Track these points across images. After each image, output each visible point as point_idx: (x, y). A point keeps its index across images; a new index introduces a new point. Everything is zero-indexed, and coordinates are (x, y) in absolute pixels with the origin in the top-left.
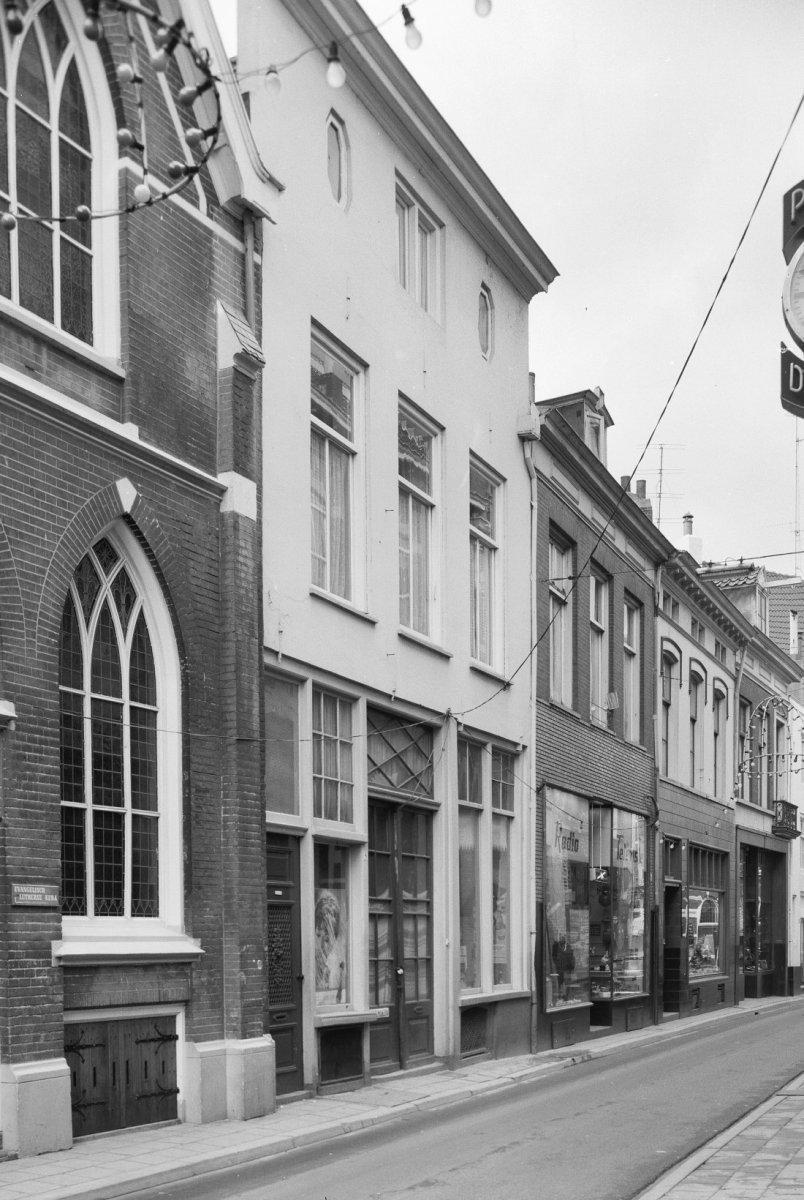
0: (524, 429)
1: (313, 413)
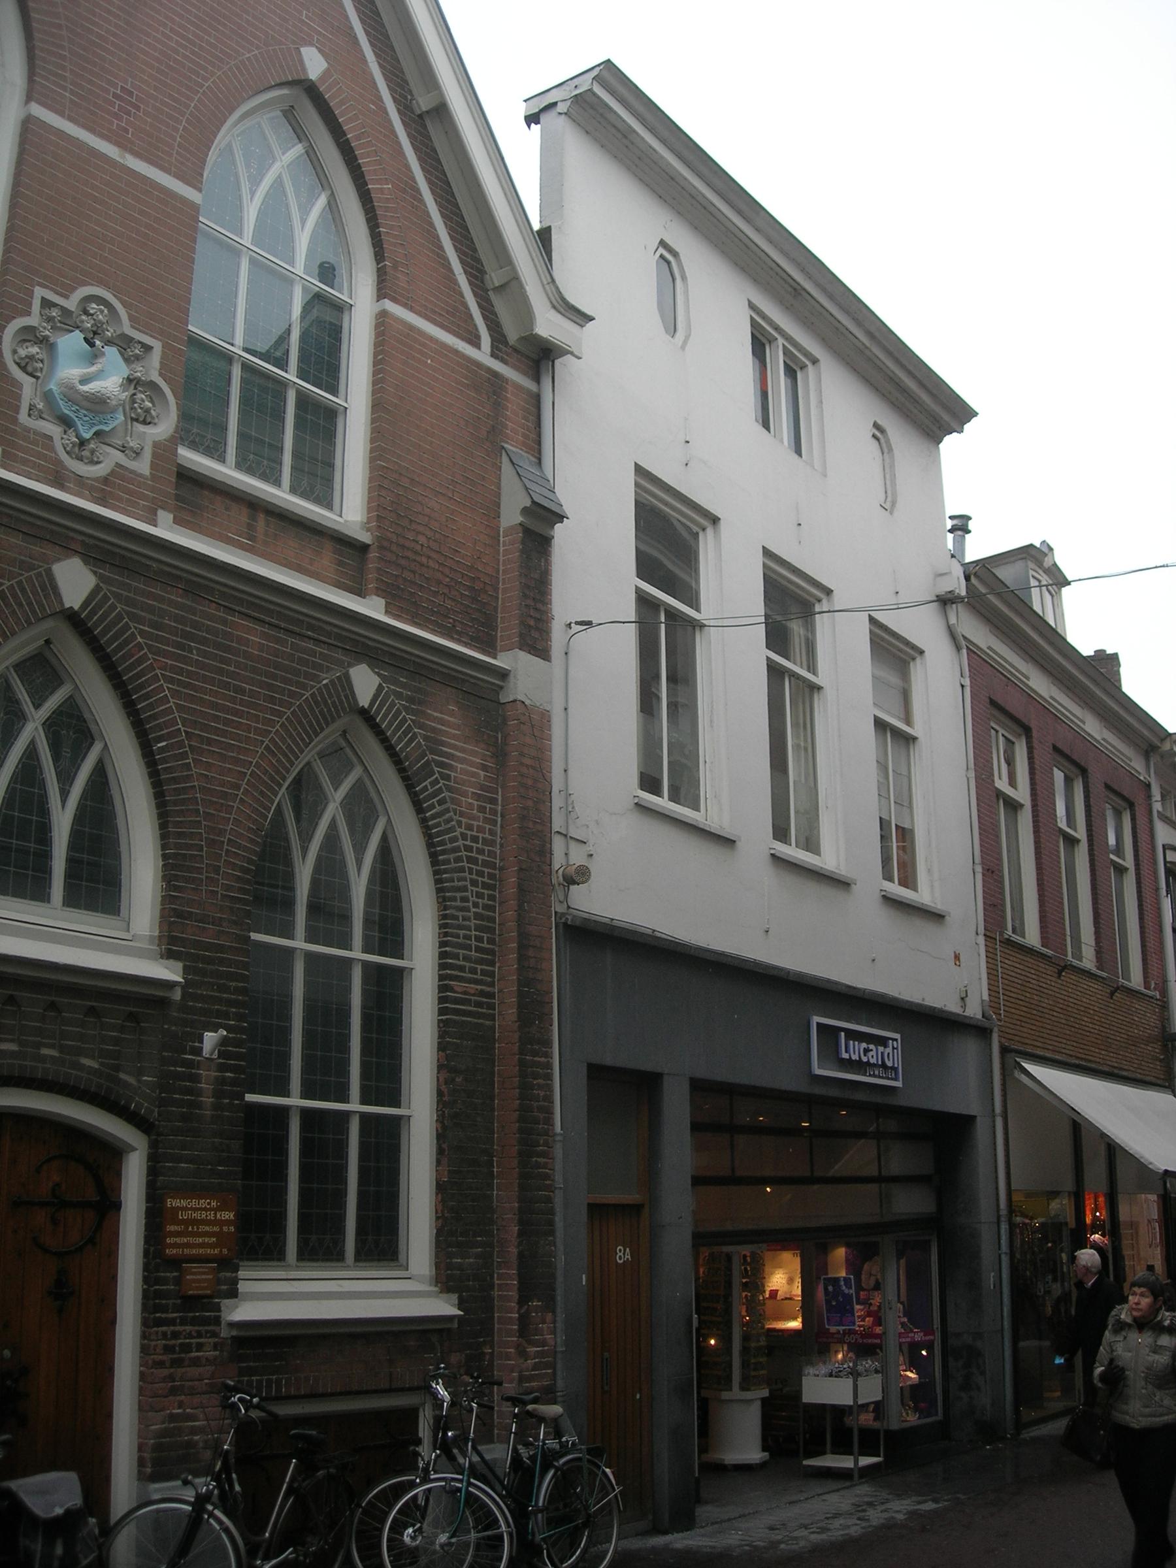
0: (944, 587)
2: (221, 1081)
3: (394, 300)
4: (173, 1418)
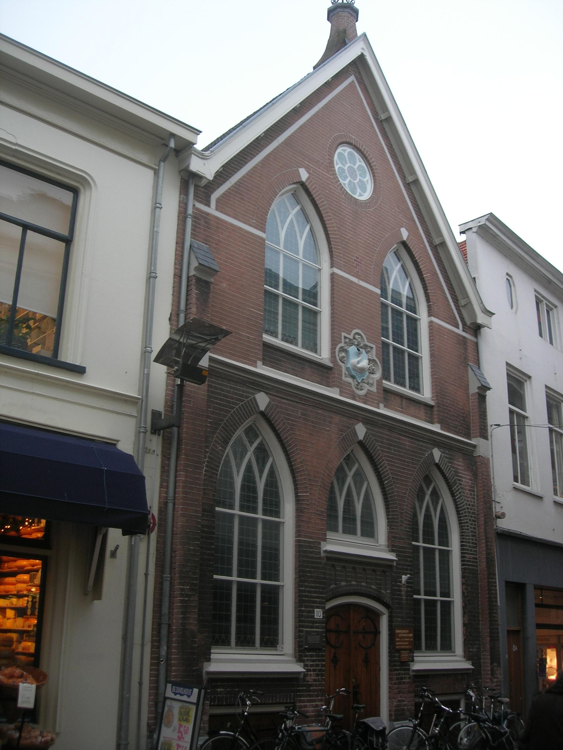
1: (509, 403)
2: (407, 591)
3: (434, 317)
4: (399, 701)
